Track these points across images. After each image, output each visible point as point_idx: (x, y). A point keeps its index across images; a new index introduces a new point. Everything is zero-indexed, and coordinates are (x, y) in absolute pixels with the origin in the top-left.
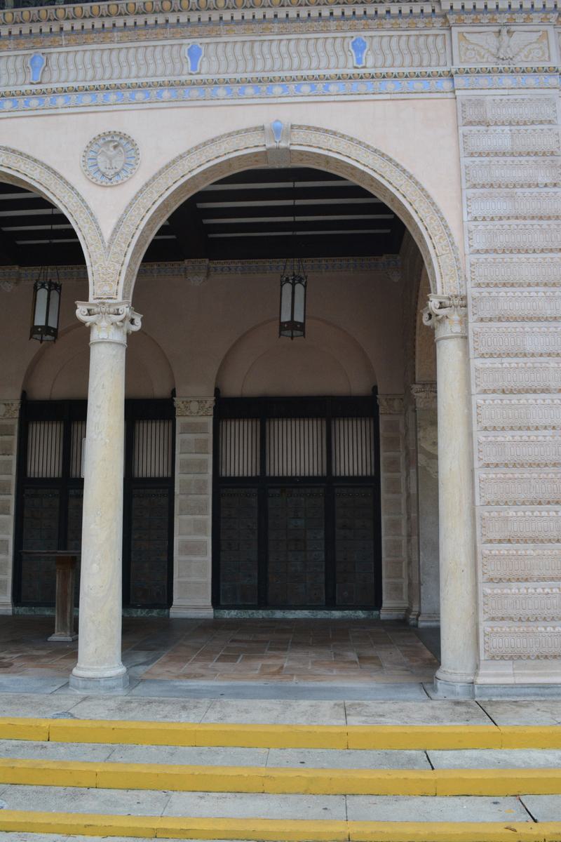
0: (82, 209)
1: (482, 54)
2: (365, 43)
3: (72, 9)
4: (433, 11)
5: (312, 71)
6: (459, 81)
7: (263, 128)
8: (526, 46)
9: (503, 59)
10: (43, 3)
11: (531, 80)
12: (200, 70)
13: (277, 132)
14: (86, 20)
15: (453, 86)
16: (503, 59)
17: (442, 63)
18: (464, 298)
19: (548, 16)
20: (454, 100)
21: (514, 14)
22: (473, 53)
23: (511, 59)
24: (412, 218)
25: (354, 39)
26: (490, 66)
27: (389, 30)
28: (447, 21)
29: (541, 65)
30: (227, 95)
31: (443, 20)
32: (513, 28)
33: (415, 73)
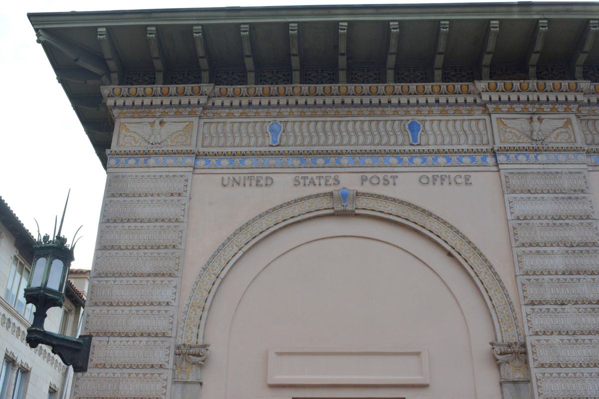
0: (222, 255)
2: (419, 125)
3: (142, 89)
5: (360, 147)
6: (501, 158)
9: (536, 140)
11: (170, 161)
12: (280, 142)
14: (318, 97)
15: (497, 161)
17: (485, 142)
18: (524, 345)
19: (570, 107)
20: (497, 173)
21: (542, 105)
22: (130, 138)
23: (159, 144)
25: (410, 122)
26: (526, 145)
28: (487, 109)
31: (484, 109)
32: (165, 119)
33: (222, 152)
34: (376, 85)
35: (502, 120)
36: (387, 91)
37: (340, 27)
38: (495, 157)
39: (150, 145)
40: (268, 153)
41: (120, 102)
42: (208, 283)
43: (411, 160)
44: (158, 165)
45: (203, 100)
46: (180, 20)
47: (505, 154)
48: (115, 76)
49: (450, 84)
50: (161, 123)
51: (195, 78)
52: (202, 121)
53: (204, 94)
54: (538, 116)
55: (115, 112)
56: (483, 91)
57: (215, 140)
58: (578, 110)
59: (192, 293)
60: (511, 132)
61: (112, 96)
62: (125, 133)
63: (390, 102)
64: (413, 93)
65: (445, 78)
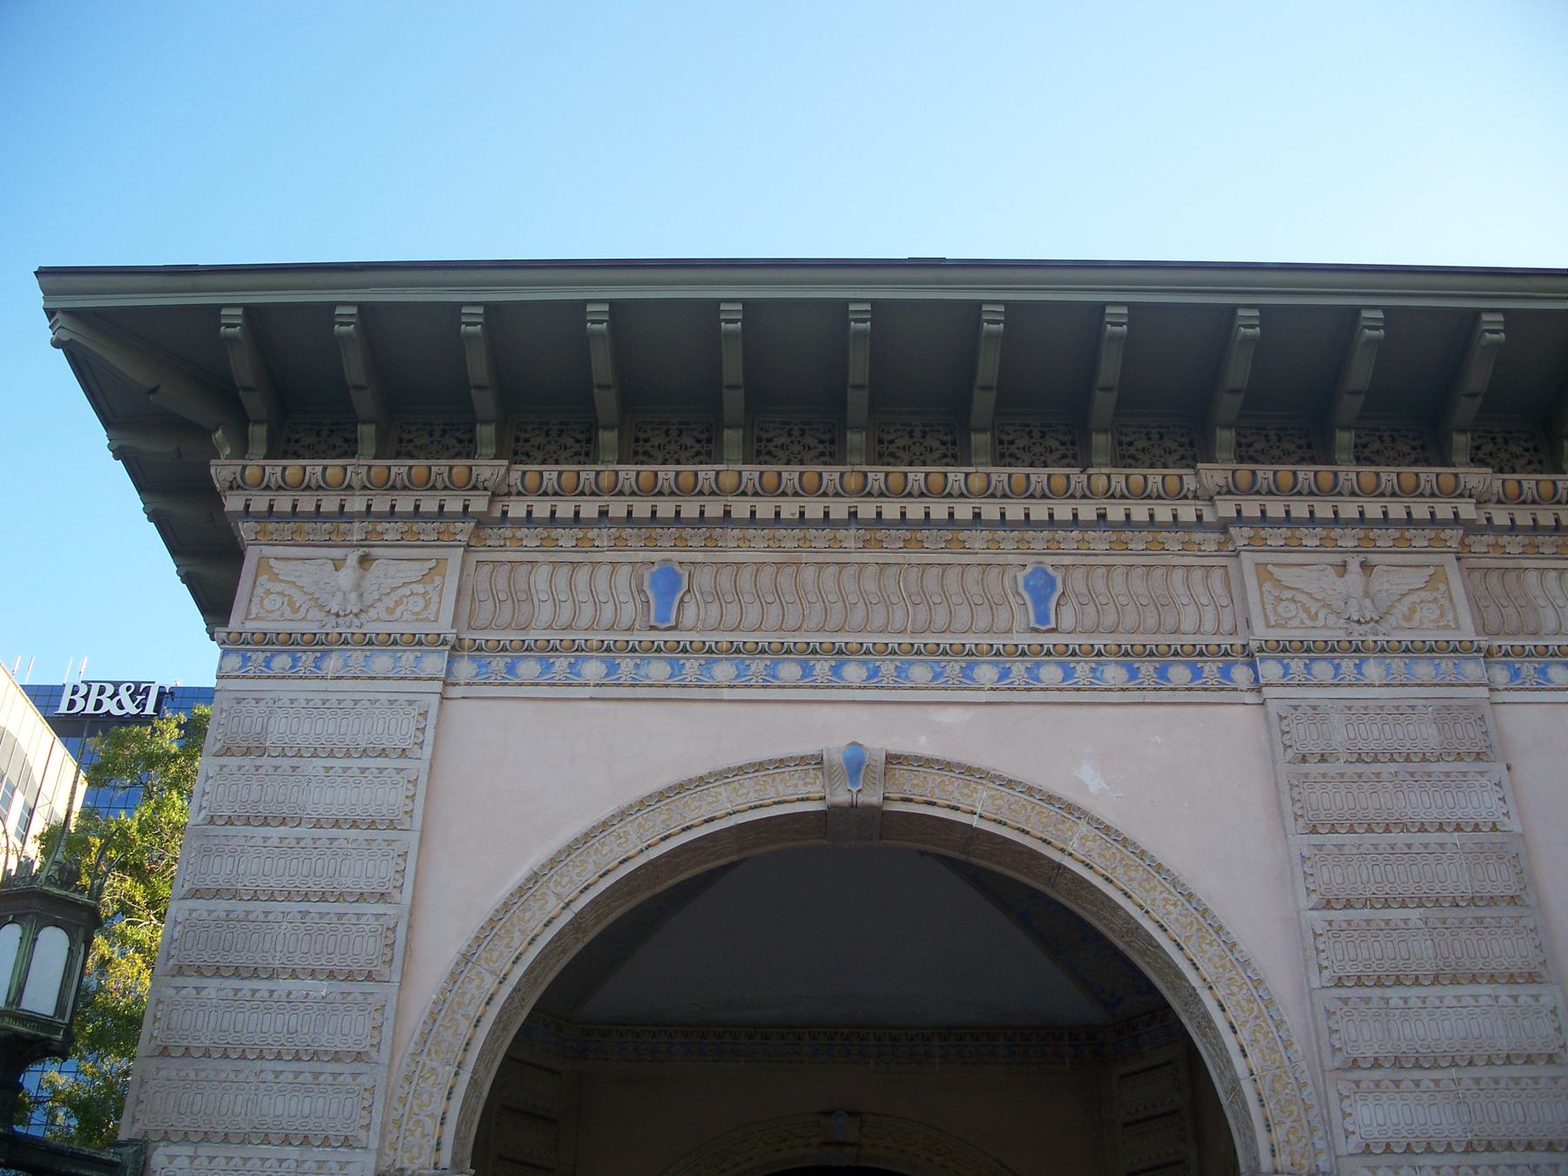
1: (1313, 610)
4: (1199, 517)
7: (819, 760)
8: (1404, 595)
10: (1049, 461)
13: (856, 765)
15: (1256, 679)
16: (1358, 622)
24: (1184, 978)
27: (941, 551)
29: (1443, 636)
30: (803, 677)
34: (1374, 469)
35: (1270, 568)
36: (972, 486)
37: (464, 319)
38: (1253, 666)
39: (333, 620)
40: (1114, 649)
41: (260, 504)
42: (473, 997)
43: (1162, 673)
44: (1397, 682)
45: (479, 504)
46: (368, 286)
47: (1280, 660)
48: (258, 432)
49: (770, 469)
50: (364, 560)
51: (460, 441)
52: (473, 558)
53: (480, 485)
54: (1361, 557)
55: (246, 530)
56: (1219, 493)
57: (507, 608)
58: (1462, 543)
59: (430, 1023)
60: (281, 594)
61: (239, 487)
62: (269, 585)
63: (1102, 516)
64: (916, 491)
65: (1002, 456)
